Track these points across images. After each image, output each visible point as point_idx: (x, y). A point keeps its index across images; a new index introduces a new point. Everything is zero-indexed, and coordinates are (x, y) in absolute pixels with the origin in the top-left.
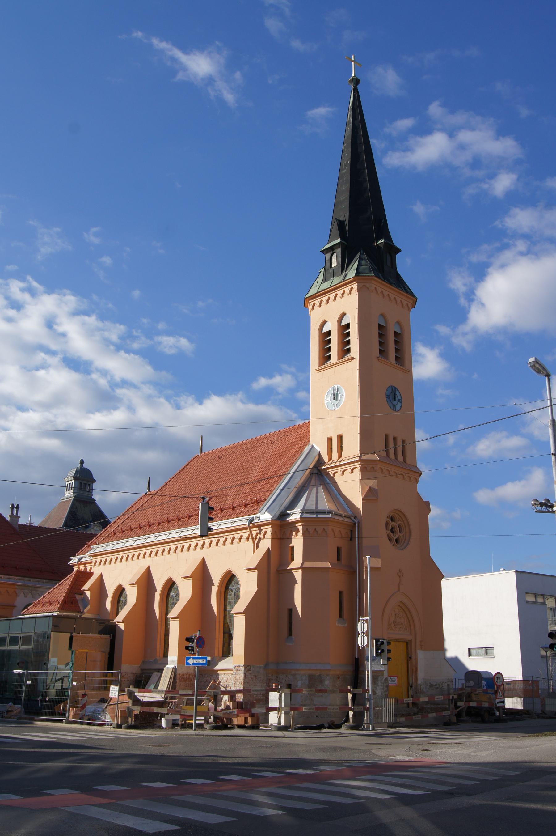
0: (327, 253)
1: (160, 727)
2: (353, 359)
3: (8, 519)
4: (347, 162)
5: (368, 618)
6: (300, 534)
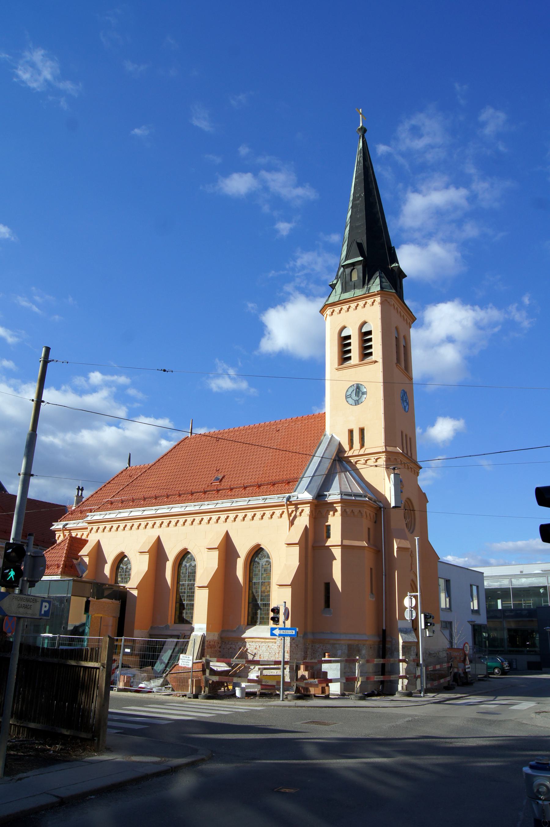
0: (347, 268)
1: (232, 695)
2: (376, 362)
4: (360, 195)
5: (418, 594)
6: (338, 514)
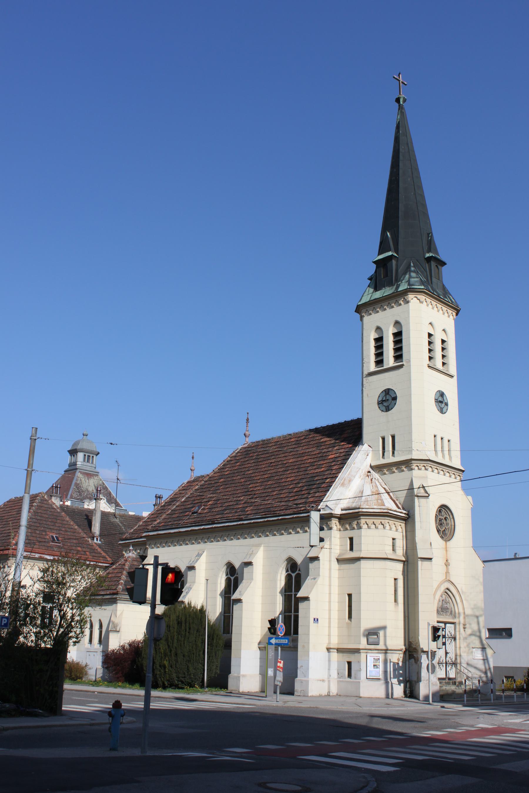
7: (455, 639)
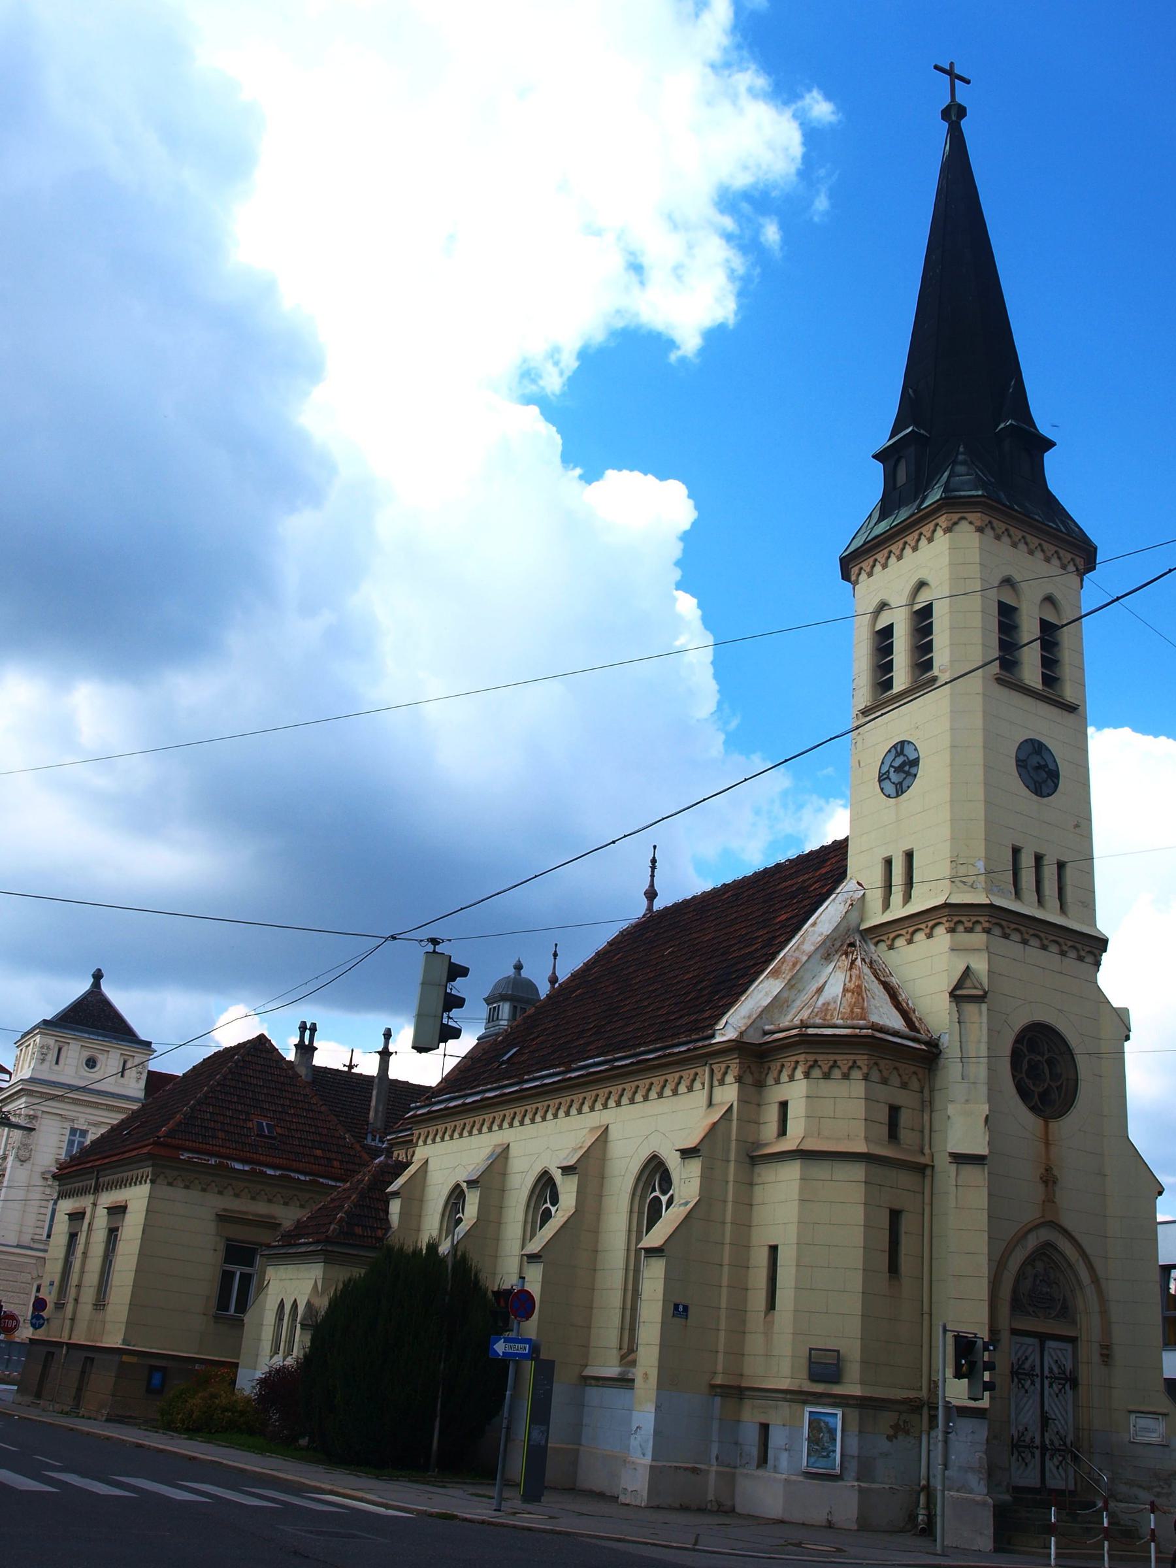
3: (290, 1055)
7: (1074, 1383)
